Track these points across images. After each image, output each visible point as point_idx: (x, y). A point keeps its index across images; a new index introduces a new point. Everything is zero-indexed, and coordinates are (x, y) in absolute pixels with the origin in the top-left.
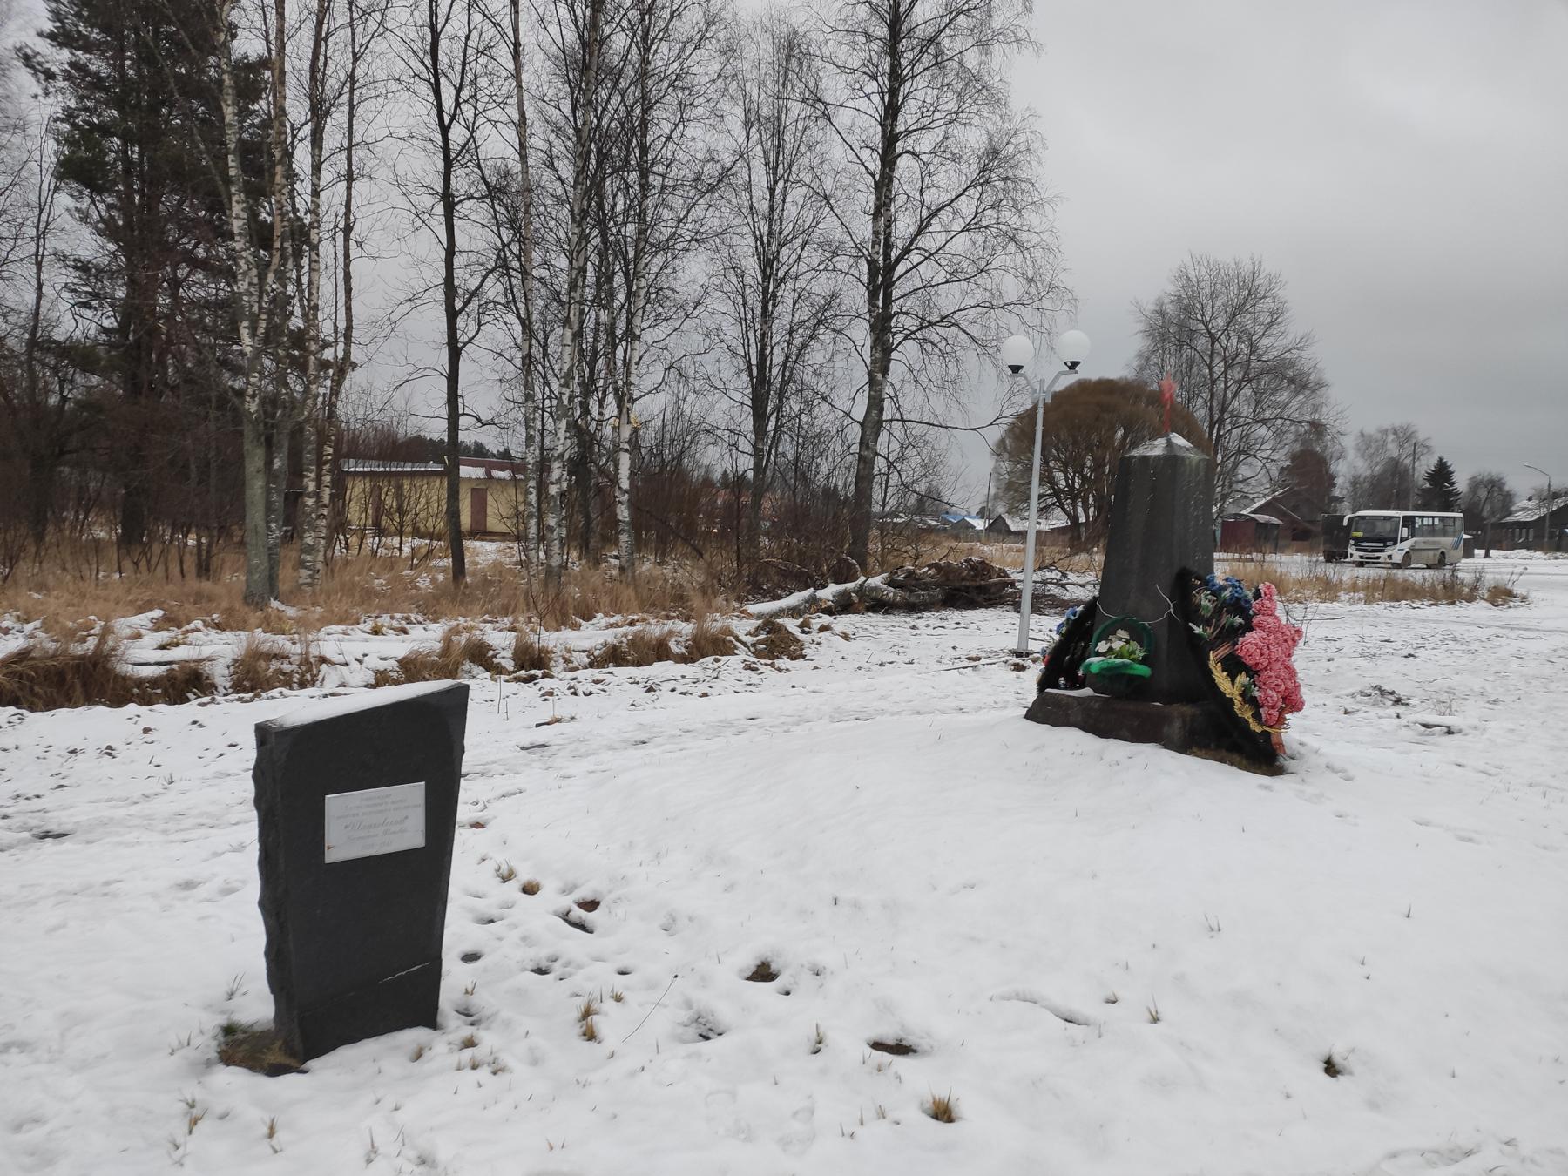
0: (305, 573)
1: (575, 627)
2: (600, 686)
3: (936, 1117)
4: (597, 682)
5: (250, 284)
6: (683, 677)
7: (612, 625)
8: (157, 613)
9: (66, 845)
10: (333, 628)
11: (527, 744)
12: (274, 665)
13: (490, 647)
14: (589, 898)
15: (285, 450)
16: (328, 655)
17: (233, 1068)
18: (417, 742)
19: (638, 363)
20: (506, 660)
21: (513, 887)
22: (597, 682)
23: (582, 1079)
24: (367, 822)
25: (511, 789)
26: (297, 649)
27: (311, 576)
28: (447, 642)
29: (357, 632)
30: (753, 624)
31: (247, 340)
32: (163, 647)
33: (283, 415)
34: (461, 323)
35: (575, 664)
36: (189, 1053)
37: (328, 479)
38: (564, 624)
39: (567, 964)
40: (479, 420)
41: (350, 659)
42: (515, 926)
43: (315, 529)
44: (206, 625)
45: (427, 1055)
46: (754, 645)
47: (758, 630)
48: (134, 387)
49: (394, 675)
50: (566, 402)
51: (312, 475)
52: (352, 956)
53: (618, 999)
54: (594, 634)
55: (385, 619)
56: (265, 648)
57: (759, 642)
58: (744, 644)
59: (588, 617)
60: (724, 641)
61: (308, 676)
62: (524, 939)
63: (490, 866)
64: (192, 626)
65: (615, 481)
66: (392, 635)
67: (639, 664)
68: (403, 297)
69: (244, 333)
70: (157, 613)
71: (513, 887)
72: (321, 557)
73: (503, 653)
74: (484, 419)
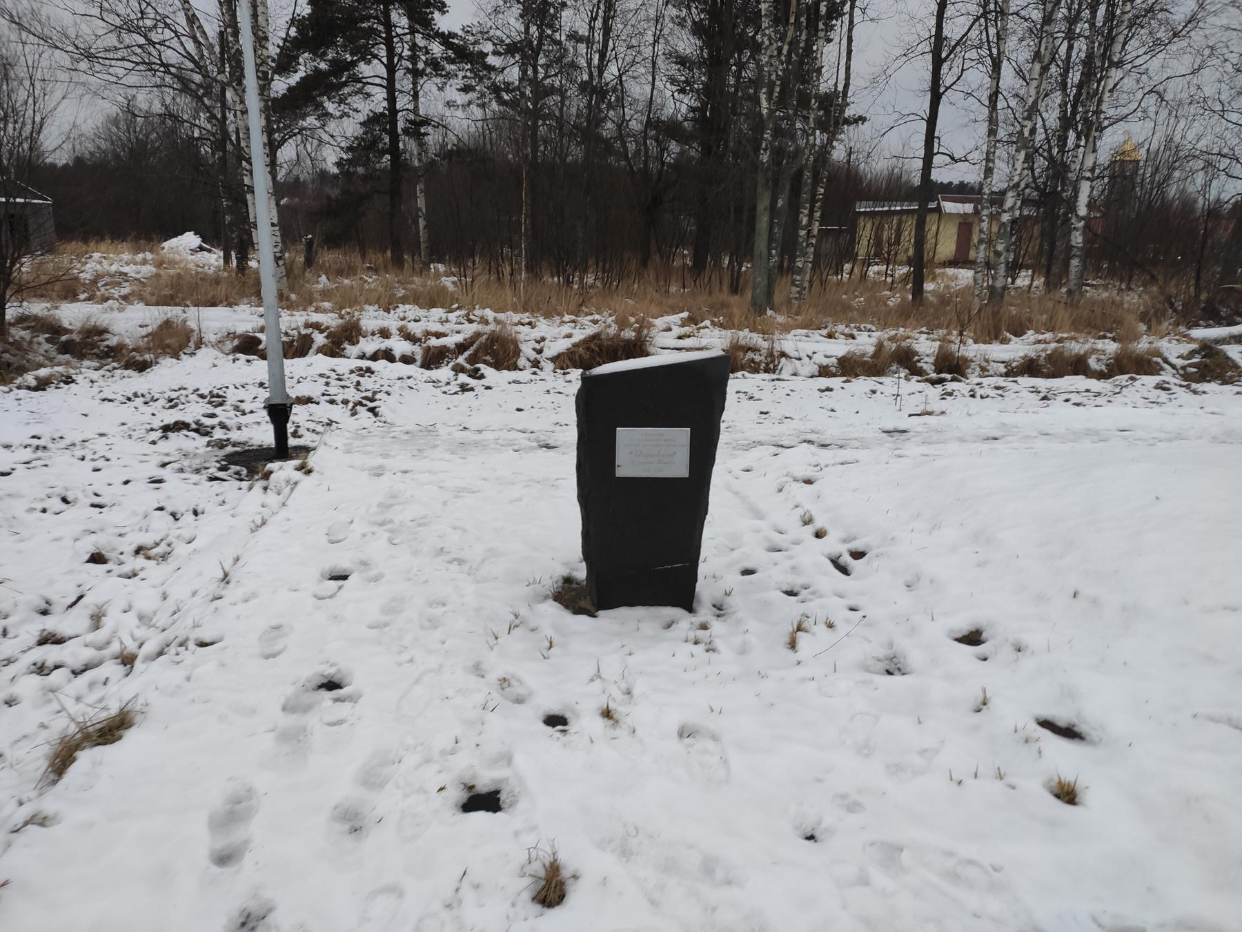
0: (795, 289)
1: (1005, 341)
2: (1000, 392)
3: (1058, 796)
4: (997, 388)
5: (771, 57)
6: (1087, 391)
7: (1039, 342)
8: (685, 315)
9: (551, 453)
10: (799, 331)
11: (891, 428)
12: (750, 355)
13: (916, 354)
14: (861, 550)
15: (787, 191)
16: (787, 351)
17: (556, 604)
18: (693, 399)
19: (1111, 91)
20: (927, 365)
21: (810, 529)
22: (997, 388)
23: (763, 673)
24: (651, 452)
25: (849, 459)
26: (766, 345)
27: (798, 292)
28: (880, 346)
29: (816, 335)
30: (1186, 348)
31: (764, 104)
32: (680, 338)
33: (788, 163)
34: (945, 68)
35: (991, 372)
36: (538, 587)
37: (818, 214)
38: (996, 338)
39: (813, 593)
40: (952, 158)
41: (803, 355)
42: (790, 557)
43: (805, 254)
44: (713, 323)
45: (674, 626)
46: (1183, 368)
47: (1192, 354)
48: (707, 150)
49: (833, 369)
50: (1026, 134)
51: (806, 212)
52: (640, 550)
53: (830, 626)
54: (1017, 349)
55: (841, 328)
56: (742, 342)
57: (1190, 365)
58: (1173, 367)
59: (1019, 333)
60: (1149, 362)
61: (771, 366)
62: (793, 568)
63: (800, 511)
64: (703, 324)
65: (1072, 208)
66: (842, 339)
67: (1054, 376)
68: (899, 52)
69: (763, 97)
70: (685, 315)
71: (810, 529)
72: (807, 277)
73: (927, 359)
74: (956, 157)
